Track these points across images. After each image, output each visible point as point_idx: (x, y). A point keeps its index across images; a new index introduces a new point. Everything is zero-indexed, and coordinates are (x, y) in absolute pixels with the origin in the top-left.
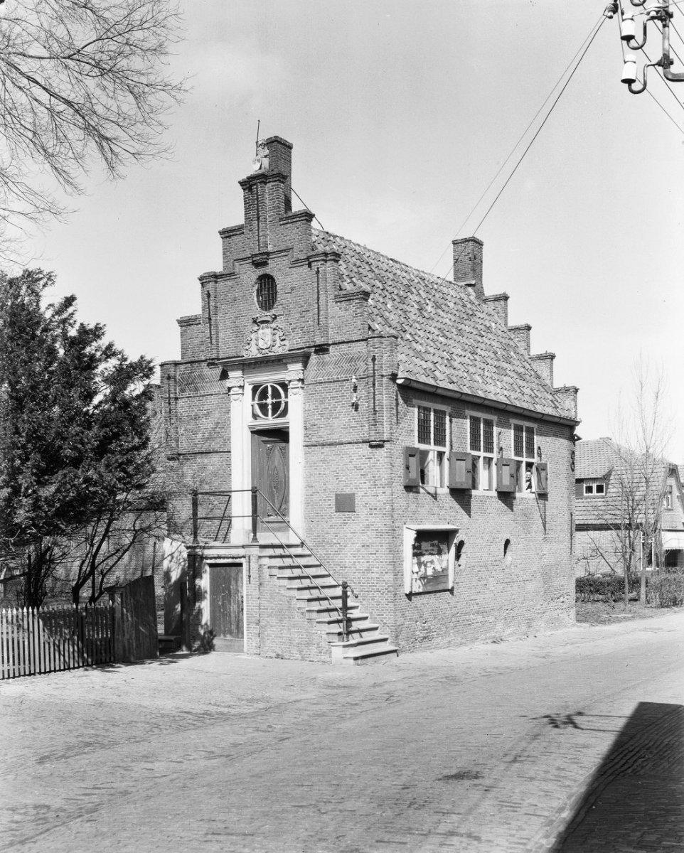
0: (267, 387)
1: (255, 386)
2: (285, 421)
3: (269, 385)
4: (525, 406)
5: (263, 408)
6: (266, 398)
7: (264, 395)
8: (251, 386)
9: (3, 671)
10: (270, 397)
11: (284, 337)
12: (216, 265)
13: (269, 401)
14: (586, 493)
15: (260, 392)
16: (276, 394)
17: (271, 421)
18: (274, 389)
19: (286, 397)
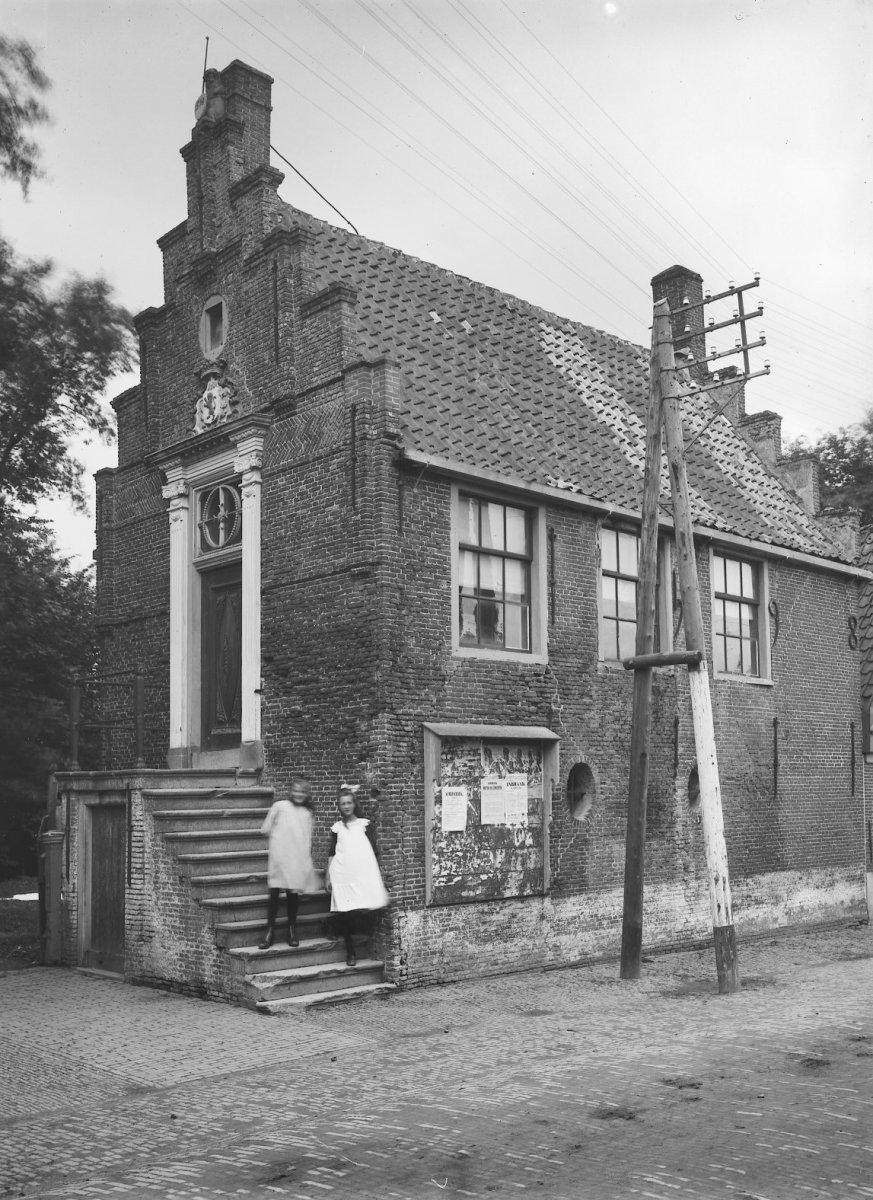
8: (199, 495)
13: (222, 512)
17: (221, 553)
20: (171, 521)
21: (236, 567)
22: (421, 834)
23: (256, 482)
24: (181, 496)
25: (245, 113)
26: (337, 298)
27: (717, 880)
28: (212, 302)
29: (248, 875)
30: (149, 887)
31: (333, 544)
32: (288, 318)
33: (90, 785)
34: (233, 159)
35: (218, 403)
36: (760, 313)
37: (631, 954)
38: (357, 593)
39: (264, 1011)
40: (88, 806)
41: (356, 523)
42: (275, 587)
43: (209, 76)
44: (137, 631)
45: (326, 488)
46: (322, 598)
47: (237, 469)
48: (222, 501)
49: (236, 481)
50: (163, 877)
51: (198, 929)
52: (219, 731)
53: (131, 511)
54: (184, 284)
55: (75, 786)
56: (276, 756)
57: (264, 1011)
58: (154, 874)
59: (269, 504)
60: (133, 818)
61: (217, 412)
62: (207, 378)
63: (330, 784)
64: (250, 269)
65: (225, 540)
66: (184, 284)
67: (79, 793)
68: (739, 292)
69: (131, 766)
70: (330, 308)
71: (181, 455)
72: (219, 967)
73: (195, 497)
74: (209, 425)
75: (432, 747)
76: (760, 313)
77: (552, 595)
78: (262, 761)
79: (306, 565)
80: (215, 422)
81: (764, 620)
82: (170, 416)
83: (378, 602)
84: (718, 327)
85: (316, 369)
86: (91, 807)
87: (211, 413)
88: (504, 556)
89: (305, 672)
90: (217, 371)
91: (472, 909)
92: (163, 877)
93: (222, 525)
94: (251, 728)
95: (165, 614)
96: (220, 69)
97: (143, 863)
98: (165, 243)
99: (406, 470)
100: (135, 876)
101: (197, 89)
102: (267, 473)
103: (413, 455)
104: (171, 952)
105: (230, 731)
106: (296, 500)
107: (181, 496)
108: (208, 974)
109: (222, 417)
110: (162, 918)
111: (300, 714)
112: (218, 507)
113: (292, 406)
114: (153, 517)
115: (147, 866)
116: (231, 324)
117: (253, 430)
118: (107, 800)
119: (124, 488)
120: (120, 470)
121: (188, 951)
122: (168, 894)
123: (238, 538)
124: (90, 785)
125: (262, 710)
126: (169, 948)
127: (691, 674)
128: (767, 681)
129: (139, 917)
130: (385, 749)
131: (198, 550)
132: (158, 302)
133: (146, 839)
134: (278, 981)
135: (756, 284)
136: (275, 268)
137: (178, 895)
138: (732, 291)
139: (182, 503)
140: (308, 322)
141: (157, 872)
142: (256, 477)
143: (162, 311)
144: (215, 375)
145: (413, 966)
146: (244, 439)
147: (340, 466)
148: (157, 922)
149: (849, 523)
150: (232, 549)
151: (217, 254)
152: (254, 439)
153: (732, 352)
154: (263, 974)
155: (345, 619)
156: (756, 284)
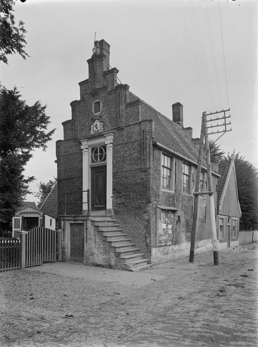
0: (98, 148)
1: (92, 148)
2: (105, 162)
3: (98, 147)
4: (198, 206)
5: (96, 158)
6: (100, 156)
7: (96, 152)
8: (91, 149)
9: (1, 249)
10: (99, 152)
11: (104, 126)
12: (78, 97)
13: (99, 154)
14: (20, 219)
15: (94, 150)
16: (101, 151)
17: (99, 163)
18: (101, 149)
19: (106, 152)
20: (83, 154)
21: (104, 168)
22: (156, 231)
23: (112, 147)
24: (86, 148)
25: (105, 53)
26: (138, 103)
27: (215, 241)
28: (97, 101)
29: (119, 240)
30: (93, 243)
31: (135, 163)
32: (123, 107)
33: (72, 218)
34: (104, 65)
35: (99, 126)
36: (230, 117)
37: (192, 257)
38: (143, 175)
39: (131, 271)
40: (70, 223)
41: (144, 158)
42: (117, 172)
43: (96, 43)
44: (71, 181)
45: (134, 149)
46: (132, 176)
47: (106, 143)
48: (99, 150)
49: (105, 147)
50: (97, 240)
51: (109, 253)
52: (97, 206)
53: (68, 151)
54: (87, 95)
55: (66, 218)
56: (116, 212)
57: (131, 271)
58: (94, 240)
59: (115, 152)
60: (88, 226)
61: (99, 129)
62: (95, 120)
63: (134, 219)
64: (110, 93)
65: (100, 160)
66: (87, 95)
67: (67, 220)
68: (224, 111)
69: (63, 214)
70: (136, 106)
71: (88, 138)
72: (116, 261)
73: (90, 149)
74: (96, 132)
75: (159, 211)
76: (230, 117)
77: (175, 177)
78: (113, 213)
79: (127, 168)
80: (98, 131)
81: (204, 185)
82: (82, 128)
83: (149, 177)
84: (219, 119)
85: (130, 120)
86: (71, 224)
87: (97, 128)
88: (167, 168)
89: (126, 193)
90: (99, 118)
91: (163, 247)
92: (97, 240)
93: (99, 156)
94: (109, 205)
95: (81, 177)
96: (99, 40)
97: (91, 237)
98: (81, 84)
99: (155, 146)
100: (88, 240)
101: (93, 46)
102: (115, 145)
103: (158, 144)
104: (100, 258)
105: (100, 206)
106: (124, 152)
107: (86, 148)
108: (113, 263)
109: (100, 130)
110: (97, 250)
111: (124, 203)
112: (99, 152)
113: (123, 129)
114: (76, 153)
115: (92, 238)
116: (103, 107)
117: (112, 134)
118: (77, 222)
119: (66, 145)
120: (64, 141)
121: (106, 258)
122: (99, 244)
123: (105, 159)
124: (72, 218)
125: (113, 202)
126: (100, 257)
127: (210, 197)
128: (205, 199)
129: (90, 250)
130: (150, 211)
131: (91, 162)
132: (78, 98)
133: (92, 231)
134: (133, 264)
135: (229, 110)
136: (119, 94)
137: (103, 245)
138: (223, 111)
139: (87, 150)
140: (128, 108)
141: (95, 239)
142: (111, 145)
143: (80, 102)
144: (98, 119)
145: (155, 261)
146: (108, 136)
147: (138, 144)
148: (95, 251)
149: (216, 164)
150: (103, 162)
151: (99, 89)
152: (112, 136)
153: (222, 125)
154: (129, 263)
155: (138, 181)
156: (229, 110)
